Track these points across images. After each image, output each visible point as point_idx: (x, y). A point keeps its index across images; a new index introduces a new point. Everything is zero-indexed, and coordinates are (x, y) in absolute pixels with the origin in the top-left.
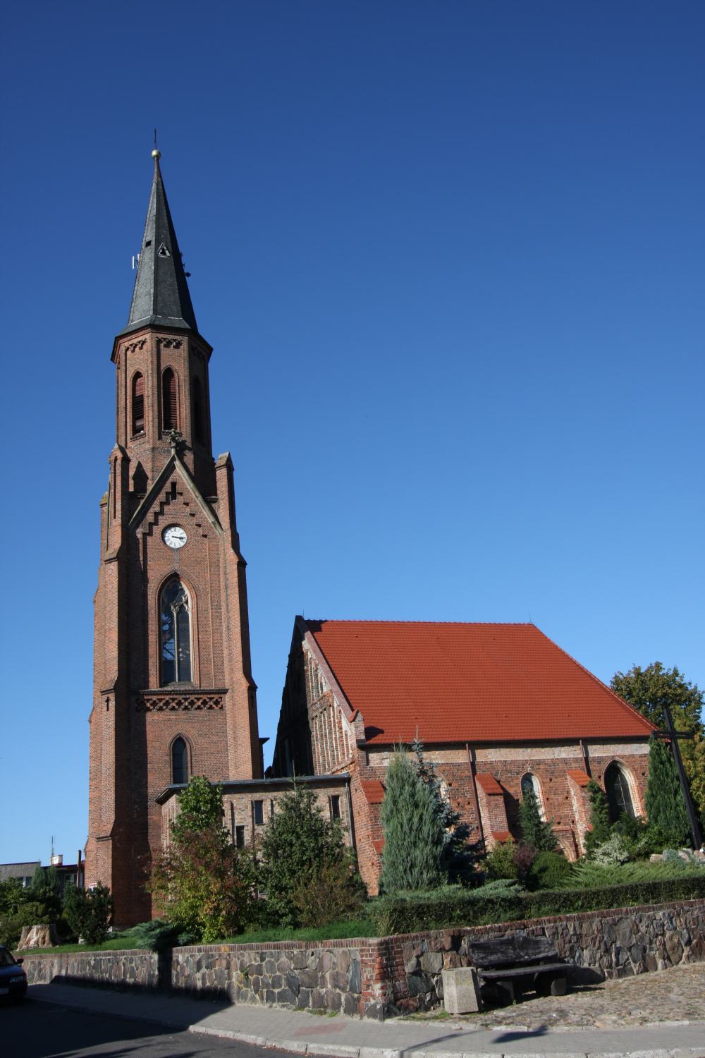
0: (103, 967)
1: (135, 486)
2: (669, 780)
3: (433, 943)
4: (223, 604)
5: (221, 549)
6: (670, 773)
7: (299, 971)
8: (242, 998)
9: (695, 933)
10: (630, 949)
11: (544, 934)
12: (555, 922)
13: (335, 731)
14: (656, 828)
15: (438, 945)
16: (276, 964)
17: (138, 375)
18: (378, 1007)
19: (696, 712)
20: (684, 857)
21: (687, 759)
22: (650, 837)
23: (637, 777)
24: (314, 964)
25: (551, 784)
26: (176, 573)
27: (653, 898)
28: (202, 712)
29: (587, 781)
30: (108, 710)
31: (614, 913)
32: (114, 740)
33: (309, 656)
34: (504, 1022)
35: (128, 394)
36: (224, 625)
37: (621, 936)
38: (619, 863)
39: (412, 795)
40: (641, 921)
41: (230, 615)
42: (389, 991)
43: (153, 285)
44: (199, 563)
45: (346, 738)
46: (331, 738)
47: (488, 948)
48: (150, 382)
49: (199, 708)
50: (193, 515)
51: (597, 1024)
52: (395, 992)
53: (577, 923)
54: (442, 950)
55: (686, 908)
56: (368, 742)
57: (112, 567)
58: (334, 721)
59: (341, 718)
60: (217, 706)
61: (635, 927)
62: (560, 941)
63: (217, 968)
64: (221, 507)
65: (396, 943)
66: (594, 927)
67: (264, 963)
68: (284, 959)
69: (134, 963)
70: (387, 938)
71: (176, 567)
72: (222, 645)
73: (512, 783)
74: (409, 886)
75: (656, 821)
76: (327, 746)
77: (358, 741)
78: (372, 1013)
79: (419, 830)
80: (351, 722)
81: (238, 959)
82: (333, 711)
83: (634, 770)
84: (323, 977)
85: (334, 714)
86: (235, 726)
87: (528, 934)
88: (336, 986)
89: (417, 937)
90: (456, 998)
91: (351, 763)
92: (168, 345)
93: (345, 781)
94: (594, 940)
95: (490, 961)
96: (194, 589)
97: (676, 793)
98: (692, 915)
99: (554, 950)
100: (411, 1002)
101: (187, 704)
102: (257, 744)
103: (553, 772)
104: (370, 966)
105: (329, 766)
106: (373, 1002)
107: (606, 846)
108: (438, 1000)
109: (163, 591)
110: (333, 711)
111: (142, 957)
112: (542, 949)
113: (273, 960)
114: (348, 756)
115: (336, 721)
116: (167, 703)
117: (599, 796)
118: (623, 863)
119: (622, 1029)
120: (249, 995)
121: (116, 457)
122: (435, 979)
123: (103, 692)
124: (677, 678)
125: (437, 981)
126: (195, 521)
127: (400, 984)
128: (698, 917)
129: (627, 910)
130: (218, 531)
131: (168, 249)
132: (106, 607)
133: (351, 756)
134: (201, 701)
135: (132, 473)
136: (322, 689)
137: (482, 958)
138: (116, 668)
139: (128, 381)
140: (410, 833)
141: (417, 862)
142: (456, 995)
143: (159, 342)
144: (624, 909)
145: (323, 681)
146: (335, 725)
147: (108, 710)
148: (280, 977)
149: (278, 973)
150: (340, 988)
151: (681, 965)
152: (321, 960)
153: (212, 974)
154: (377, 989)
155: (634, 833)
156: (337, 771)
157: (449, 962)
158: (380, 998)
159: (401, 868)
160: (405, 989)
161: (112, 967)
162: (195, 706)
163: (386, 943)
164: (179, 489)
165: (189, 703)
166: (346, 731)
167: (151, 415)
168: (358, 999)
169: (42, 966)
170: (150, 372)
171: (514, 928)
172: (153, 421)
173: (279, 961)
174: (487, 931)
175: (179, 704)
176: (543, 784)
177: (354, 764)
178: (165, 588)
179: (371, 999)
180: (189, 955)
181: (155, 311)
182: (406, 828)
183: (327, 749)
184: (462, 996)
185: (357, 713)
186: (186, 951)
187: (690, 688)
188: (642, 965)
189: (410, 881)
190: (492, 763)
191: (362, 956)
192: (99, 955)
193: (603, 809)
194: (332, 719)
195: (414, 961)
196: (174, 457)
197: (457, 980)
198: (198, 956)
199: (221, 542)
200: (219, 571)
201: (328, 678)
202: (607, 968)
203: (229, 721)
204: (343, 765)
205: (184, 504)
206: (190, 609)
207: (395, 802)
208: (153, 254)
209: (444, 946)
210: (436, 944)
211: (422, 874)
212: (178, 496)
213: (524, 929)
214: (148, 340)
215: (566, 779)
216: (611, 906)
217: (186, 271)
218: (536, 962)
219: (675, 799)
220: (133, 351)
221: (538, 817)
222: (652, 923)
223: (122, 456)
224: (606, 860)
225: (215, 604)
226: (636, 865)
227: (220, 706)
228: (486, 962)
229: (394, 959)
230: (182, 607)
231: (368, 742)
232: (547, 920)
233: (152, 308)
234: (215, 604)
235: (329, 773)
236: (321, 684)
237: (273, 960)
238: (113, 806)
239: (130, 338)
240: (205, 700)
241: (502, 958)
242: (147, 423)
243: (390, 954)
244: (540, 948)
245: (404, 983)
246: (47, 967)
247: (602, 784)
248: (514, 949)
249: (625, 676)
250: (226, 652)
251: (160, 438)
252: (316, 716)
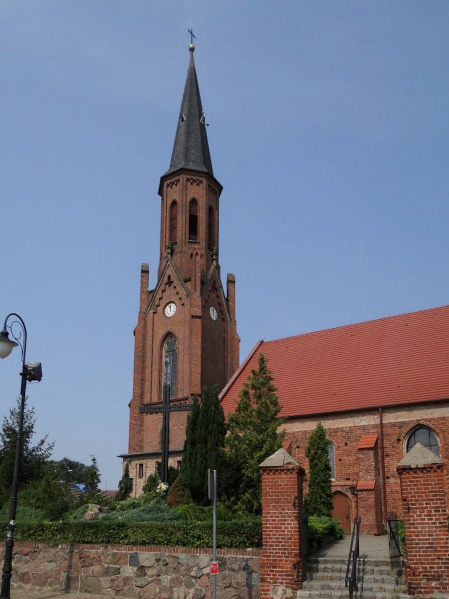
25: (346, 448)
103: (349, 438)
190: (294, 433)
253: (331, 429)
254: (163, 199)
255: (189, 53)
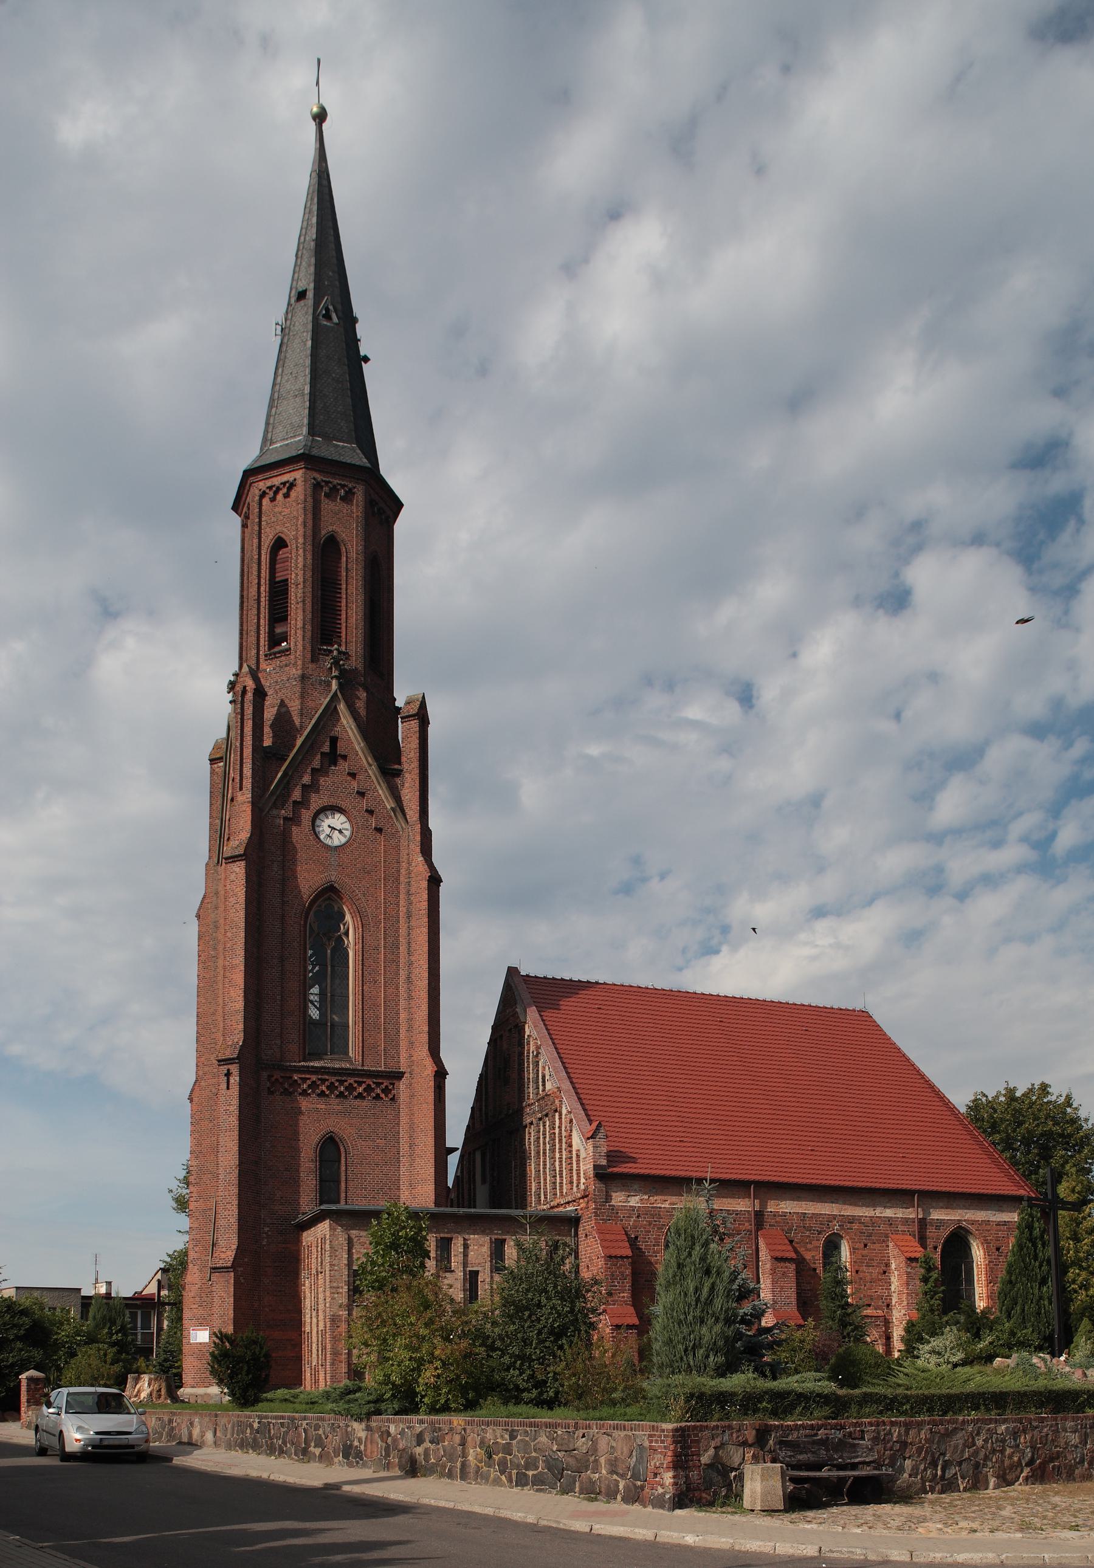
0: (272, 1432)
1: (275, 736)
2: (1037, 1264)
3: (735, 1435)
4: (403, 941)
5: (404, 853)
6: (1041, 1254)
7: (563, 1453)
8: (482, 1479)
9: (1040, 1452)
10: (960, 1464)
11: (863, 1439)
12: (878, 1425)
13: (560, 1149)
14: (1007, 1325)
15: (740, 1438)
16: (532, 1444)
17: (280, 544)
18: (667, 1496)
19: (1087, 1163)
20: (1039, 1365)
21: (1068, 1238)
22: (997, 1336)
23: (988, 1252)
24: (585, 1447)
25: (865, 1252)
26: (332, 886)
27: (997, 1408)
28: (365, 1103)
29: (919, 1253)
30: (228, 1088)
31: (949, 1422)
32: (237, 1133)
33: (527, 1033)
34: (815, 1521)
35: (263, 575)
36: (403, 974)
37: (952, 1448)
38: (950, 1366)
39: (703, 1259)
40: (978, 1434)
41: (413, 959)
42: (682, 1481)
43: (308, 379)
44: (368, 873)
45: (578, 1161)
46: (553, 1158)
47: (798, 1446)
48: (301, 559)
49: (360, 1096)
50: (361, 794)
51: (920, 1530)
52: (688, 1482)
53: (903, 1429)
54: (744, 1444)
55: (1035, 1424)
56: (610, 1170)
57: (237, 870)
58: (560, 1133)
59: (571, 1130)
60: (386, 1096)
61: (970, 1440)
62: (880, 1447)
63: (446, 1443)
64: (407, 785)
65: (693, 1431)
66: (923, 1436)
67: (514, 1442)
68: (543, 1439)
69: (321, 1429)
70: (679, 1425)
71: (333, 876)
72: (397, 1005)
73: (809, 1246)
74: (689, 1370)
75: (1009, 1317)
76: (545, 1168)
77: (596, 1167)
78: (658, 1503)
79: (709, 1302)
80: (588, 1139)
81: (478, 1435)
82: (560, 1118)
83: (986, 1242)
84: (596, 1461)
85: (561, 1123)
86: (412, 1128)
87: (844, 1435)
88: (613, 1472)
89: (717, 1426)
90: (759, 1494)
91: (583, 1198)
92: (331, 494)
93: (574, 1221)
94: (919, 1450)
95: (799, 1460)
96: (359, 913)
97: (1043, 1282)
98: (1040, 1432)
99: (872, 1456)
100: (704, 1495)
101: (342, 1089)
102: (442, 1152)
103: (870, 1235)
104: (661, 1453)
105: (546, 1198)
106: (660, 1490)
107: (936, 1343)
108: (739, 1496)
109: (312, 913)
110: (560, 1118)
111: (333, 1424)
112: (859, 1454)
113: (527, 1439)
114: (577, 1186)
115: (564, 1134)
116: (313, 1085)
117: (935, 1275)
118: (955, 1366)
119: (946, 1536)
120: (492, 1476)
121: (245, 687)
122: (733, 1474)
123: (222, 1062)
124: (1069, 1110)
125: (735, 1476)
126: (365, 804)
127: (694, 1475)
128: (1047, 1435)
129: (964, 1420)
130: (400, 824)
131: (336, 311)
132: (226, 932)
133: (582, 1187)
134: (364, 1086)
135: (270, 714)
136: (544, 1085)
137: (790, 1457)
138: (241, 1026)
139: (263, 552)
140: (697, 1305)
141: (704, 1341)
142: (760, 1491)
143: (317, 486)
144: (961, 1418)
145: (547, 1073)
146: (560, 1141)
147: (228, 1088)
148: (536, 1458)
149: (534, 1454)
150: (617, 1474)
151: (1016, 1486)
152: (595, 1442)
153: (438, 1449)
154: (668, 1477)
155: (975, 1330)
156: (558, 1206)
157: (750, 1458)
158: (671, 1487)
159: (681, 1347)
160: (699, 1481)
161: (286, 1433)
162: (355, 1094)
163: (682, 1429)
164: (341, 749)
165: (346, 1088)
166: (578, 1150)
167: (300, 617)
168: (642, 1488)
169: (175, 1424)
170: (301, 540)
171: (829, 1427)
172: (304, 627)
173: (536, 1441)
174: (797, 1428)
175: (332, 1087)
176: (853, 1250)
177: (586, 1199)
178: (314, 909)
179: (659, 1487)
180: (405, 1426)
181: (312, 430)
182: (691, 1299)
183: (545, 1172)
184: (765, 1494)
185: (599, 1126)
186: (401, 1421)
187: (1085, 1127)
188: (970, 1481)
189: (692, 1363)
191: (651, 1442)
192: (266, 1417)
193: (936, 1293)
194: (557, 1131)
195: (711, 1452)
196: (335, 694)
197: (763, 1475)
198: (419, 1428)
199: (404, 843)
200: (398, 888)
201: (555, 1068)
202: (930, 1482)
203: (404, 1119)
204: (569, 1199)
205: (349, 774)
206: (352, 945)
207: (680, 1266)
208: (310, 318)
209: (747, 1440)
210: (738, 1437)
211: (707, 1357)
212: (341, 761)
213: (840, 1430)
214: (299, 482)
215: (888, 1246)
216: (945, 1413)
217: (362, 353)
218: (854, 1466)
219: (1039, 1289)
220: (273, 500)
221: (844, 1296)
222: (992, 1438)
223: (254, 686)
224: (934, 1359)
225: (390, 940)
226: (977, 1368)
227: (391, 1096)
228: (794, 1461)
229: (690, 1447)
230: (340, 940)
231: (610, 1170)
232: (868, 1423)
233: (306, 421)
234: (390, 940)
235: (545, 1207)
236: (544, 1077)
237: (527, 1439)
238: (235, 1227)
239: (268, 475)
240: (369, 1085)
241: (812, 1459)
242: (293, 632)
243: (686, 1442)
244: (858, 1452)
245: (698, 1475)
246: (184, 1426)
247: (937, 1257)
248: (827, 1450)
249: (990, 1099)
250: (403, 1016)
251: (314, 659)
252: (531, 1123)
253: (843, 1215)
254: (244, 526)
255: (312, 126)
